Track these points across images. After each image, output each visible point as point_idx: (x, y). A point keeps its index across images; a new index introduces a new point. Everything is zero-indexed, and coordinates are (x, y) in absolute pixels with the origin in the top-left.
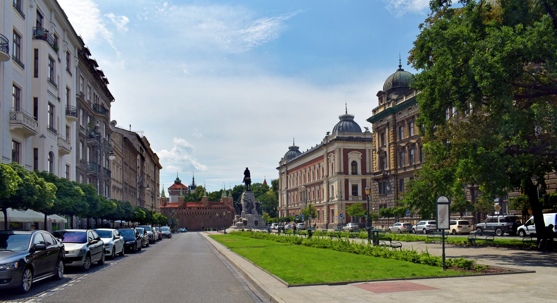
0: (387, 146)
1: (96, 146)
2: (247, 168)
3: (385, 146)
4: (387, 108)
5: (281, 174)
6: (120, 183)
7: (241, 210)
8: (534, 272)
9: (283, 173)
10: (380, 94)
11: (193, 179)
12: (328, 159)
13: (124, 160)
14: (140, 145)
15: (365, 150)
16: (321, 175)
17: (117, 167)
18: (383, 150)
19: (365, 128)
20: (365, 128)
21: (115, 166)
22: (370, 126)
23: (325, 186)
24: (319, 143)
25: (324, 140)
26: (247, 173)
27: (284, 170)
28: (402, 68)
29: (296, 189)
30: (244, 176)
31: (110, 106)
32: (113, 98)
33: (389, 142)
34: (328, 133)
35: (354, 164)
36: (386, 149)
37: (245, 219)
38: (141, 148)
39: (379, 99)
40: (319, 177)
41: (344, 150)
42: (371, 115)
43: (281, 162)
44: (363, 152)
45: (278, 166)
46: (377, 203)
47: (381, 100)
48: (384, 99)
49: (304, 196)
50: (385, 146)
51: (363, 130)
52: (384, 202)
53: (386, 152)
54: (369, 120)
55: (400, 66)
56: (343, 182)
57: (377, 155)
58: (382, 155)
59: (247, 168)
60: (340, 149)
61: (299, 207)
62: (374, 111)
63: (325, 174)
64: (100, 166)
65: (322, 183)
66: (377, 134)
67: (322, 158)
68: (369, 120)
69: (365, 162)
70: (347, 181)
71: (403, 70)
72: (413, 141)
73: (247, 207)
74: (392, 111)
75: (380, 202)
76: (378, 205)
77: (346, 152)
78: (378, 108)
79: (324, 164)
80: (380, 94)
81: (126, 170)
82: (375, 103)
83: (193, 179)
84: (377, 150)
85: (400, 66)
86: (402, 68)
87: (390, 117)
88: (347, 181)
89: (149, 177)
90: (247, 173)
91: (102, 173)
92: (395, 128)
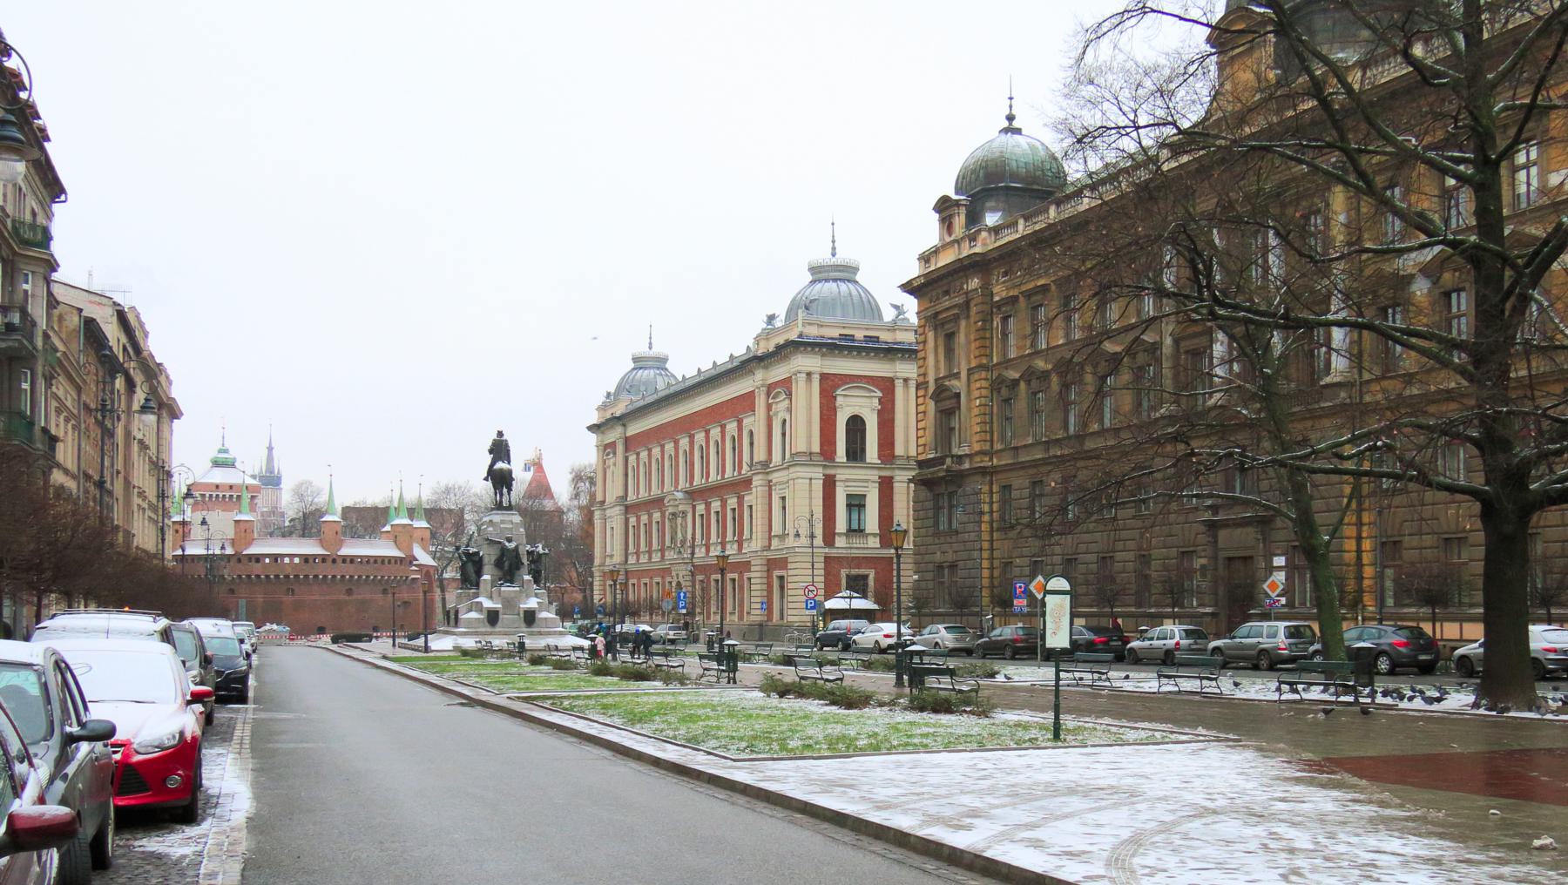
0: (964, 375)
1: (19, 359)
2: (500, 434)
3: (957, 376)
4: (965, 254)
5: (607, 449)
6: (74, 477)
7: (479, 573)
8: (751, 433)
9: (613, 445)
10: (944, 207)
11: (270, 449)
12: (769, 407)
13: (84, 397)
14: (124, 339)
15: (891, 381)
16: (746, 458)
17: (67, 420)
18: (947, 389)
19: (896, 307)
20: (896, 307)
21: (62, 418)
22: (911, 304)
23: (754, 497)
24: (740, 351)
25: (757, 340)
26: (500, 449)
27: (615, 435)
28: (1016, 124)
29: (658, 502)
30: (488, 458)
31: (49, 216)
32: (63, 191)
33: (969, 362)
34: (771, 318)
35: (856, 426)
36: (958, 385)
37: (488, 604)
38: (125, 348)
39: (942, 220)
40: (738, 464)
41: (824, 377)
42: (913, 270)
43: (602, 408)
44: (886, 386)
45: (595, 419)
46: (927, 558)
47: (947, 223)
48: (959, 221)
49: (684, 528)
50: (957, 376)
51: (889, 315)
52: (950, 557)
53: (958, 395)
54: (910, 288)
55: (1010, 118)
56: (818, 485)
57: (931, 404)
58: (947, 404)
59: (500, 434)
60: (809, 374)
61: (666, 564)
62: (925, 258)
63: (760, 455)
64: (31, 424)
65: (747, 483)
66: (931, 335)
67: (745, 403)
68: (910, 288)
69: (892, 421)
70: (829, 484)
71: (1018, 131)
72: (1040, 364)
73: (499, 564)
74: (978, 265)
75: (938, 557)
76: (931, 566)
77: (830, 386)
78: (936, 251)
79: (755, 422)
80: (944, 207)
81: (87, 429)
82: (930, 233)
83: (270, 449)
84: (931, 390)
85: (1010, 118)
86: (1016, 124)
87: (974, 283)
88: (829, 484)
89: (147, 448)
90: (500, 449)
91: (39, 445)
92: (987, 319)
